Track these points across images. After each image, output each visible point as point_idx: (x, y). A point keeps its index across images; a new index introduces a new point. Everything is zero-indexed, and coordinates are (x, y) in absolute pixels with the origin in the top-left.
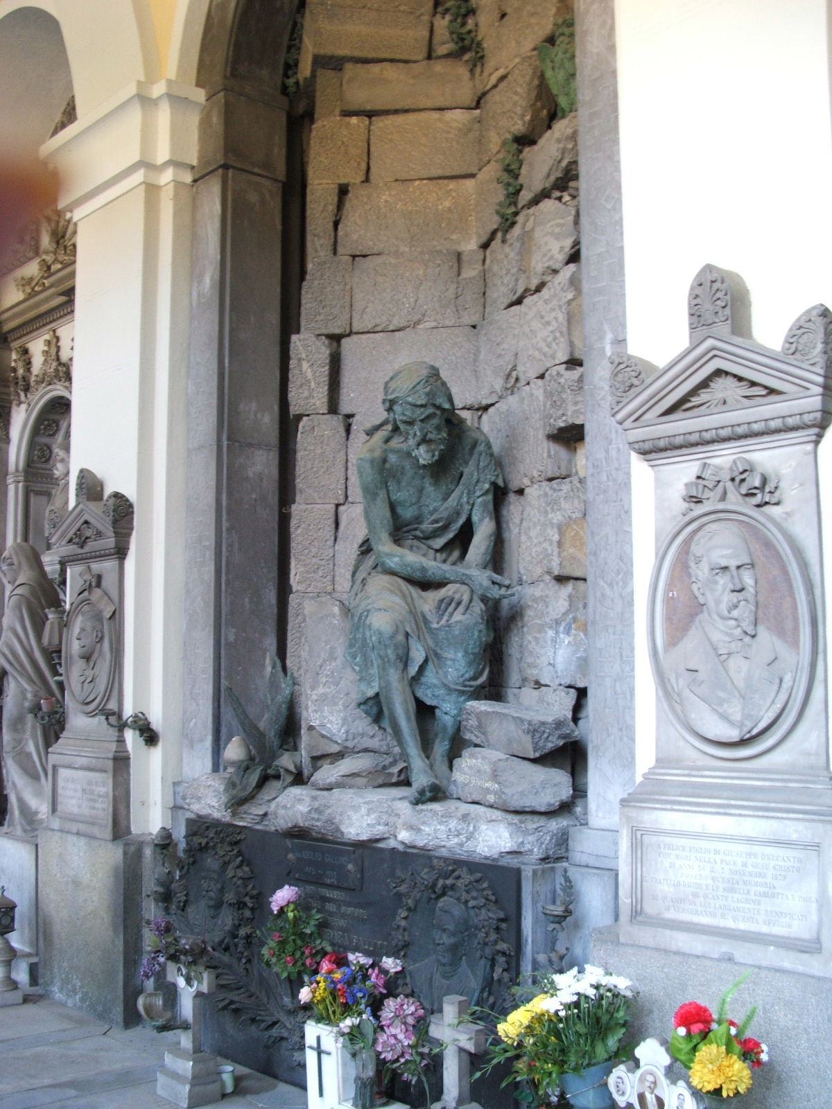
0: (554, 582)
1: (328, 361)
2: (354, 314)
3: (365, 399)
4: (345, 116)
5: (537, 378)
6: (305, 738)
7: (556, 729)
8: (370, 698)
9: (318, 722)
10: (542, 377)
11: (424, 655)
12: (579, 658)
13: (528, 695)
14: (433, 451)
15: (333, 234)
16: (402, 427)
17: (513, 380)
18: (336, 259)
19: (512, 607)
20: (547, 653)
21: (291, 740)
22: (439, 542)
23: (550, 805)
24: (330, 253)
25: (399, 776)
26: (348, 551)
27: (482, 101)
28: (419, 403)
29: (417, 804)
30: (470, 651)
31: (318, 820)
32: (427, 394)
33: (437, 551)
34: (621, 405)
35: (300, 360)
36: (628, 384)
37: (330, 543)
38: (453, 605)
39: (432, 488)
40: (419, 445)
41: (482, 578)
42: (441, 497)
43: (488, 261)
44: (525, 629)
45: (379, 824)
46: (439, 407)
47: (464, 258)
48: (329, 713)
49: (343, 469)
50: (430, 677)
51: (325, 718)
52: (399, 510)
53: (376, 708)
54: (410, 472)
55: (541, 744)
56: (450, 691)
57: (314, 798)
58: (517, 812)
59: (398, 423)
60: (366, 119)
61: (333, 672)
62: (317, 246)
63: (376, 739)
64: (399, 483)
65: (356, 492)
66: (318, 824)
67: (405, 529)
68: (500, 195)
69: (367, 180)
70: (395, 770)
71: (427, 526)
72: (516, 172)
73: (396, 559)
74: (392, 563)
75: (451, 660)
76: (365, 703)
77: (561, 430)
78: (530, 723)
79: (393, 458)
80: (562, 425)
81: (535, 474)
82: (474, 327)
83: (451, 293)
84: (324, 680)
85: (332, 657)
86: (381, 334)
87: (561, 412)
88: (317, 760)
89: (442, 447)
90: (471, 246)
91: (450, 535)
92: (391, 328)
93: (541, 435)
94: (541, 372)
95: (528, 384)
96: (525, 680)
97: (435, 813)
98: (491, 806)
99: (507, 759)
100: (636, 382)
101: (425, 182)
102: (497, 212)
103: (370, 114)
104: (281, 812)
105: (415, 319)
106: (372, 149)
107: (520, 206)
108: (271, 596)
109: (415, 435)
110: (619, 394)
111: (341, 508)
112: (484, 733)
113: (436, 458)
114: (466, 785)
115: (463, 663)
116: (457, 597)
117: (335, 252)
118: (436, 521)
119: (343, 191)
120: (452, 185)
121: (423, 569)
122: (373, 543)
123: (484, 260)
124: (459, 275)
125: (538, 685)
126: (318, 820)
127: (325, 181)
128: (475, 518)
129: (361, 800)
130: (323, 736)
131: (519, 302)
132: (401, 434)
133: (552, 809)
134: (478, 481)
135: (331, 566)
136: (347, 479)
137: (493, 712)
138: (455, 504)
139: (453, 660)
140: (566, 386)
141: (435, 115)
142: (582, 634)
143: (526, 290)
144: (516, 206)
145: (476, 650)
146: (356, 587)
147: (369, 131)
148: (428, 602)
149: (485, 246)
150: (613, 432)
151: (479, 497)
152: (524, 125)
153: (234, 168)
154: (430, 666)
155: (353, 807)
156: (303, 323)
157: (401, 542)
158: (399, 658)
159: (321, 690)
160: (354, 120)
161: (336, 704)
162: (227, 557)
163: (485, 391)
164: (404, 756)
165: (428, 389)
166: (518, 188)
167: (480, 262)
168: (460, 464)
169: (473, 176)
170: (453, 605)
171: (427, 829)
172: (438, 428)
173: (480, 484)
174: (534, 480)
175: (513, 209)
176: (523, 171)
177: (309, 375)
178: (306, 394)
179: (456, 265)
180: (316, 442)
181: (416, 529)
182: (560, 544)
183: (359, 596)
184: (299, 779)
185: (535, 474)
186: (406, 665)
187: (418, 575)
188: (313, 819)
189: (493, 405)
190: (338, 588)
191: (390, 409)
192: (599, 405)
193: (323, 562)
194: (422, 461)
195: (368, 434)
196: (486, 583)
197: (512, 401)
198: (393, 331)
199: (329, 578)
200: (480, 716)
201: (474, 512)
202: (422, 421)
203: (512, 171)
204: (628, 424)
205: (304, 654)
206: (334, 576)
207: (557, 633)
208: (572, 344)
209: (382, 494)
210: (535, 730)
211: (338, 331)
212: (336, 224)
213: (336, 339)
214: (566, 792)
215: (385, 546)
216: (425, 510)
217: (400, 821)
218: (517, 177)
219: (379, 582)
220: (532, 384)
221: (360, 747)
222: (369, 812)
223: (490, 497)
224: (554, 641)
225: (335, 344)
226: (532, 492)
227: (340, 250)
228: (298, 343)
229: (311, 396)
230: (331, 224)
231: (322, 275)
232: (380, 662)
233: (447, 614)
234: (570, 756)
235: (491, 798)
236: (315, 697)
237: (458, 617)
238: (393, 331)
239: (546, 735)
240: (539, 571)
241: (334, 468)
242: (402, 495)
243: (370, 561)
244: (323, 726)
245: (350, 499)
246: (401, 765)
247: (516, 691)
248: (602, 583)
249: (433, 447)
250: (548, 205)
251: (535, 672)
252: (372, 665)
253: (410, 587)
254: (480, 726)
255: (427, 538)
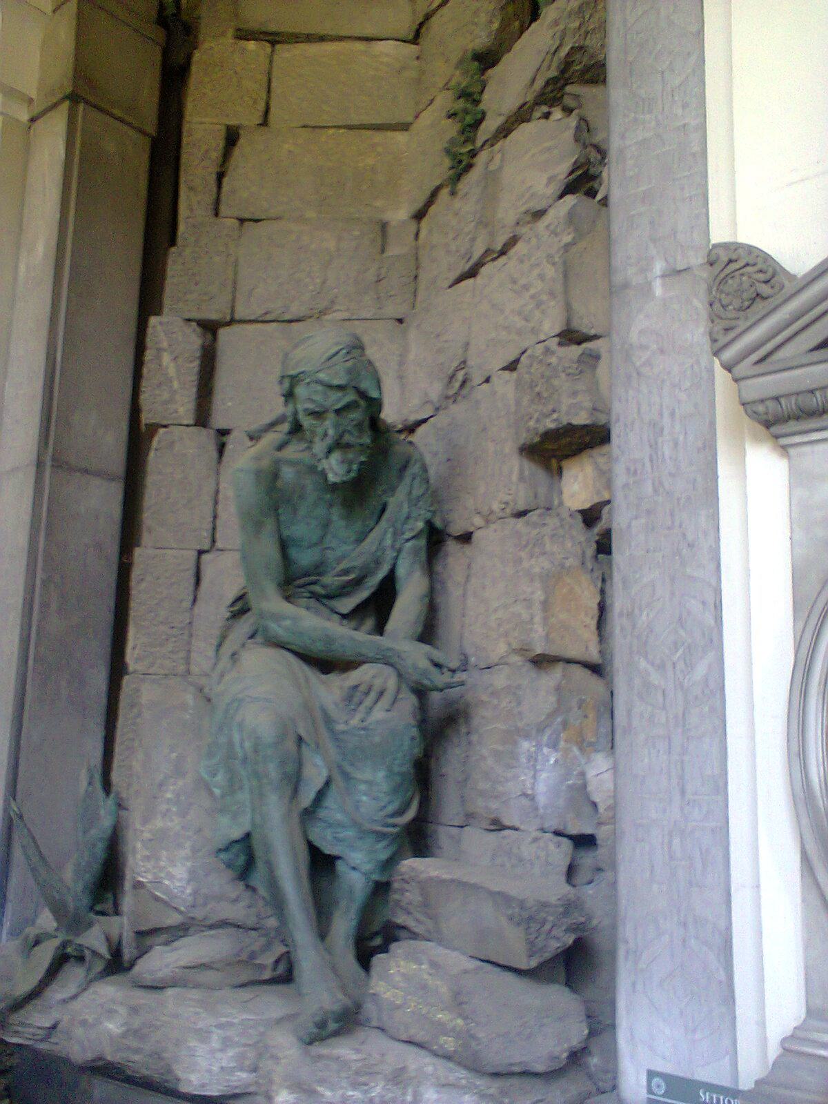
0: (528, 665)
1: (198, 354)
2: (238, 295)
3: (248, 396)
4: (240, 38)
5: (504, 369)
6: (128, 901)
7: (566, 913)
8: (236, 842)
9: (150, 877)
10: (512, 367)
11: (325, 773)
12: (570, 787)
13: (477, 841)
14: (351, 462)
15: (215, 189)
16: (306, 422)
17: (457, 385)
18: (218, 221)
19: (449, 703)
20: (521, 771)
21: (110, 895)
22: (347, 604)
23: (554, 1058)
24: (210, 213)
25: (274, 970)
26: (214, 609)
27: (423, 30)
28: (336, 382)
29: (310, 1043)
30: (396, 769)
31: (137, 1051)
32: (349, 371)
33: (344, 616)
34: (732, 335)
35: (159, 350)
36: (751, 293)
37: (187, 604)
38: (373, 695)
39: (342, 523)
40: (330, 451)
41: (417, 656)
42: (354, 537)
43: (423, 234)
44: (474, 738)
45: (241, 1070)
46: (363, 394)
47: (391, 231)
48: (170, 869)
49: (211, 504)
50: (333, 809)
51: (161, 869)
52: (293, 553)
53: (244, 858)
54: (311, 495)
55: (540, 942)
56: (363, 833)
57: (134, 1010)
58: (496, 1075)
59: (301, 416)
60: (268, 45)
61: (178, 795)
62: (192, 204)
63: (242, 904)
64: (295, 511)
65: (231, 532)
66: (136, 1057)
67: (302, 581)
68: (451, 129)
69: (265, 123)
70: (268, 959)
71: (331, 580)
72: (476, 97)
73: (288, 623)
74: (276, 629)
75: (366, 782)
76: (226, 849)
77: (548, 435)
78: (522, 904)
79: (288, 473)
80: (551, 425)
81: (496, 506)
82: (400, 321)
83: (371, 275)
84: (164, 807)
85: (179, 771)
86: (274, 325)
87: (550, 407)
88: (146, 937)
89: (363, 459)
90: (400, 214)
91: (363, 594)
92: (287, 317)
93: (510, 448)
94: (512, 358)
95: (487, 380)
96: (470, 816)
97: (343, 1064)
98: (448, 1057)
99: (477, 969)
100: (765, 290)
101: (342, 131)
102: (447, 151)
103: (274, 39)
104: (79, 1032)
105: (321, 306)
106: (274, 84)
107: (479, 144)
108: (99, 679)
109: (326, 435)
110: (731, 315)
111: (206, 558)
112: (434, 918)
113: (353, 474)
114: (399, 1007)
115: (385, 787)
116: (378, 683)
117: (217, 214)
118: (346, 572)
119: (232, 138)
120: (378, 137)
121: (329, 640)
122: (251, 597)
123: (417, 235)
124: (383, 251)
125: (497, 826)
126: (137, 1051)
127: (207, 120)
128: (401, 572)
129: (212, 1021)
130: (157, 899)
131: (472, 273)
132: (301, 440)
133: (557, 1066)
134: (408, 518)
135: (185, 637)
136: (215, 517)
137: (452, 881)
138: (374, 548)
139: (370, 783)
140: (560, 368)
141: (360, 46)
142: (575, 750)
143: (488, 252)
144: (474, 142)
145: (404, 769)
146: (221, 666)
147: (271, 62)
148: (329, 690)
149: (419, 215)
150: (666, 414)
151: (408, 540)
152: (490, 34)
153: (87, 102)
154: (333, 793)
155: (198, 1031)
156: (167, 301)
157: (292, 600)
158: (286, 776)
159: (159, 823)
160: (251, 45)
161: (180, 846)
162: (40, 621)
163: (416, 401)
164: (282, 934)
165: (349, 364)
166: (479, 116)
167: (412, 236)
168: (385, 492)
169: (405, 127)
170: (373, 695)
171: (328, 1094)
172: (359, 426)
173: (411, 521)
174: (493, 518)
175: (470, 147)
176: (486, 96)
177: (172, 371)
178: (166, 396)
179: (379, 241)
180: (177, 459)
181: (314, 583)
182: (546, 605)
183: (227, 678)
184: (116, 964)
185: (496, 506)
186: (296, 791)
187: (318, 648)
188: (129, 1048)
189: (425, 421)
190: (195, 669)
191: (289, 395)
192: (639, 374)
193: (175, 631)
194: (332, 478)
195: (252, 438)
196: (424, 664)
197: (458, 410)
198: (290, 321)
199: (182, 654)
200: (425, 886)
201: (400, 562)
202: (338, 412)
203: (470, 96)
204: (743, 368)
205: (137, 766)
206: (189, 651)
207: (539, 746)
208: (568, 308)
209: (270, 525)
210: (531, 918)
211: (214, 316)
212: (220, 176)
213: (210, 328)
214: (577, 1032)
215: (271, 602)
216: (330, 555)
217: (279, 1069)
218: (477, 102)
219: (258, 659)
220: (494, 379)
221: (214, 918)
222: (227, 1043)
223: (422, 542)
224: (533, 759)
225: (209, 336)
226: (487, 538)
227: (223, 209)
228: (159, 328)
229: (171, 400)
230: (214, 176)
231: (197, 241)
232: (255, 783)
233: (362, 708)
234: (577, 962)
235: (449, 1043)
236: (147, 835)
237: (378, 714)
238: (290, 321)
239: (548, 927)
240: (502, 648)
241: (203, 499)
242: (301, 529)
243: (244, 626)
244: (157, 882)
245: (219, 545)
246: (280, 949)
247: (455, 831)
248: (643, 664)
249: (351, 456)
250: (524, 132)
251: (494, 805)
252: (241, 788)
253: (306, 668)
254: (425, 905)
255: (330, 597)
